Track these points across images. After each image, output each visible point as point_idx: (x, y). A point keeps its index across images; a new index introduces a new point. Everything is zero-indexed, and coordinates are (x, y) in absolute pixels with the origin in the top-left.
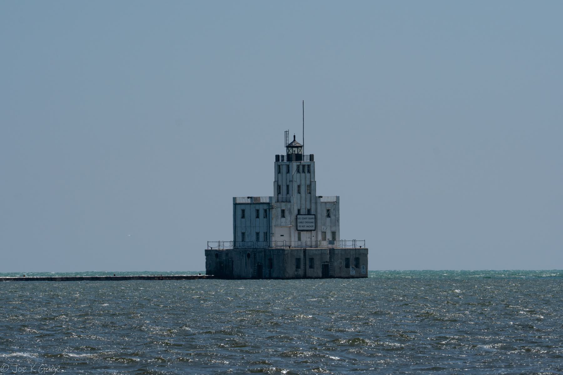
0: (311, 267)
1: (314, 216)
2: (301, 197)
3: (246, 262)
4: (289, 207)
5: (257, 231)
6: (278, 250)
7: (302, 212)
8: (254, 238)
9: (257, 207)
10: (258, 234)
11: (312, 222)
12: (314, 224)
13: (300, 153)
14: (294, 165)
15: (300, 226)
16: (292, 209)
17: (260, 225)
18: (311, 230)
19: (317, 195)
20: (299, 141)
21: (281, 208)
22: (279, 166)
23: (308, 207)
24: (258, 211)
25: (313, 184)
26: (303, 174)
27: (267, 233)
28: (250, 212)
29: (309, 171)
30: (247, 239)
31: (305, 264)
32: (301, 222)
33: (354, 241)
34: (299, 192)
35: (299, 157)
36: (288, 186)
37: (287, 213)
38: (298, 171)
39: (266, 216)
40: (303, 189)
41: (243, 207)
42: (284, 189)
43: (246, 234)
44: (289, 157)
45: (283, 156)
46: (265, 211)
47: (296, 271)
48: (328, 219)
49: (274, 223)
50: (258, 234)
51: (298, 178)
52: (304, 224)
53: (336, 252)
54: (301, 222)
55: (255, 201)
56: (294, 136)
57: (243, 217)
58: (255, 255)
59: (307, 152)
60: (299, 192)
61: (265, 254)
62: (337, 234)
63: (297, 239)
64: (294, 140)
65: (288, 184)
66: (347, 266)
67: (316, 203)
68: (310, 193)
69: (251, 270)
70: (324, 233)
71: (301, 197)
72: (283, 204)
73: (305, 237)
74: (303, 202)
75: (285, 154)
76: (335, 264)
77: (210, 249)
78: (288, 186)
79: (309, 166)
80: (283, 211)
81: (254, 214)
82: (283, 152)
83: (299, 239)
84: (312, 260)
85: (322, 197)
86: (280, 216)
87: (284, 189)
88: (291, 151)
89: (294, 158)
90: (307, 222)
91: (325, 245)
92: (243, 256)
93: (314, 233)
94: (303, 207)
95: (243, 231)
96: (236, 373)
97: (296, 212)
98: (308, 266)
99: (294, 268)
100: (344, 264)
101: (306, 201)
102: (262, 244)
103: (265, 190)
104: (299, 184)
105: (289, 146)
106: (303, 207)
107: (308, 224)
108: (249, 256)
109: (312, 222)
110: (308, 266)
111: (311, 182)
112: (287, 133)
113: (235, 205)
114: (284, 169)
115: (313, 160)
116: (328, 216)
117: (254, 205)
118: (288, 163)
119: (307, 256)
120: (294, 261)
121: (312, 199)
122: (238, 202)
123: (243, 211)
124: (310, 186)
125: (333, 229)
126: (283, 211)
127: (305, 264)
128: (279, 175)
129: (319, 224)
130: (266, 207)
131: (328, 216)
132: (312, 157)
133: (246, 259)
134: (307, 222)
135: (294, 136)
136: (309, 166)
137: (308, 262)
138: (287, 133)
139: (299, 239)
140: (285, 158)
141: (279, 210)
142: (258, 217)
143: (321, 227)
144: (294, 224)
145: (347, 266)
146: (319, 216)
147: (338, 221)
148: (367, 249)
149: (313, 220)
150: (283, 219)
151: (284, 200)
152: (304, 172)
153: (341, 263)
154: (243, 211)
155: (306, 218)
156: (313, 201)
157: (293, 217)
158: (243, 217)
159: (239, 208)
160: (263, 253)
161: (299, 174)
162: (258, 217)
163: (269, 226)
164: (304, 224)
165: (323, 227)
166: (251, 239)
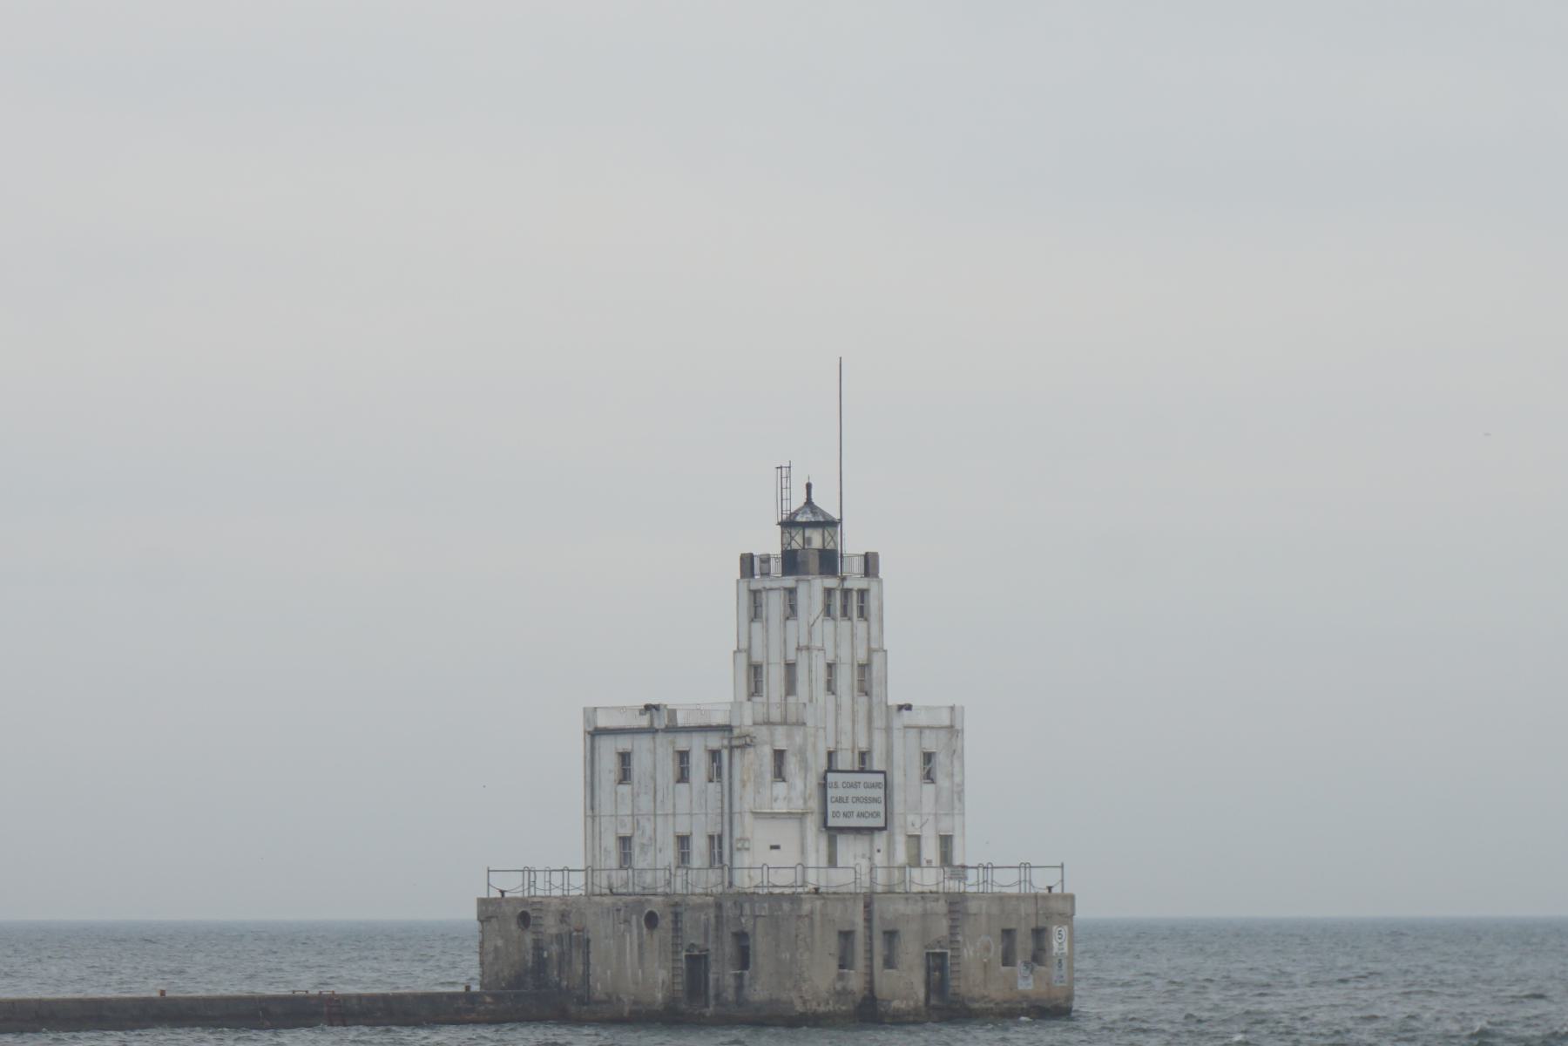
0: (889, 963)
1: (880, 778)
2: (838, 707)
3: (640, 946)
4: (798, 740)
5: (683, 831)
6: (775, 898)
7: (845, 760)
8: (669, 855)
9: (682, 742)
10: (683, 841)
11: (875, 800)
12: (880, 808)
13: (830, 546)
14: (813, 590)
15: (836, 814)
16: (810, 747)
17: (693, 808)
18: (871, 830)
19: (894, 699)
20: (826, 503)
21: (772, 744)
22: (755, 594)
23: (863, 745)
24: (683, 756)
25: (877, 660)
26: (844, 625)
27: (720, 837)
28: (653, 757)
29: (863, 613)
30: (639, 861)
31: (870, 951)
32: (840, 800)
33: (1027, 866)
34: (831, 687)
35: (829, 561)
36: (790, 667)
37: (792, 765)
38: (827, 611)
39: (719, 775)
40: (845, 678)
41: (624, 743)
42: (774, 678)
43: (636, 842)
44: (792, 562)
45: (766, 560)
46: (715, 755)
47: (841, 977)
48: (929, 789)
49: (746, 800)
50: (683, 841)
51: (833, 640)
52: (848, 807)
53: (973, 906)
54: (840, 800)
55: (657, 721)
56: (809, 486)
57: (625, 776)
58: (677, 917)
59: (853, 543)
60: (831, 687)
61: (718, 918)
62: (957, 842)
63: (823, 861)
64: (809, 502)
65: (791, 657)
66: (1008, 960)
67: (888, 730)
68: (867, 693)
69: (662, 975)
70: (915, 840)
71: (838, 707)
72: (780, 731)
73: (851, 851)
74: (846, 724)
75: (775, 549)
76: (968, 953)
77: (495, 894)
78: (790, 667)
79: (863, 593)
80: (779, 755)
81: (669, 767)
82: (770, 543)
83: (832, 861)
84: (891, 936)
85: (909, 707)
86: (769, 776)
87: (774, 678)
88: (799, 538)
89: (814, 563)
90: (858, 800)
91: (927, 878)
92: (627, 921)
93: (880, 840)
94: (846, 743)
95: (626, 832)
96: (1407, 1031)
97: (823, 762)
98: (878, 961)
99: (833, 963)
100: (997, 949)
101: (853, 722)
102: (701, 880)
103: (706, 685)
104: (830, 658)
105: (788, 524)
106: (846, 743)
107: (862, 807)
108: (651, 920)
109: (875, 800)
110: (878, 961)
111: (870, 651)
112: (784, 471)
113: (595, 733)
114: (774, 605)
115: (876, 575)
116: (929, 777)
117: (670, 737)
118: (789, 582)
119: (876, 922)
120: (833, 943)
121: (875, 714)
122: (602, 722)
123: (625, 758)
124: (864, 668)
125: (945, 828)
126: (779, 755)
127: (870, 951)
128: (757, 626)
129: (898, 808)
130: (715, 741)
131: (929, 777)
132: (870, 564)
133: (640, 935)
134: (858, 800)
135: (809, 486)
136: (863, 593)
137: (879, 945)
138: (784, 471)
139: (832, 861)
140: (776, 567)
141: (767, 751)
142: (683, 777)
143: (906, 820)
144: (814, 804)
145: (1008, 960)
146: (897, 778)
147: (960, 794)
148: (1072, 898)
149: (879, 793)
150: (780, 788)
151: (776, 715)
152: (845, 613)
153: (988, 949)
154: (625, 758)
155: (854, 785)
156: (879, 722)
157: (813, 780)
158: (625, 776)
159: (608, 750)
160: (712, 913)
161: (829, 625)
162: (683, 777)
163: (729, 814)
164: (848, 807)
165: (910, 818)
166: (655, 866)
